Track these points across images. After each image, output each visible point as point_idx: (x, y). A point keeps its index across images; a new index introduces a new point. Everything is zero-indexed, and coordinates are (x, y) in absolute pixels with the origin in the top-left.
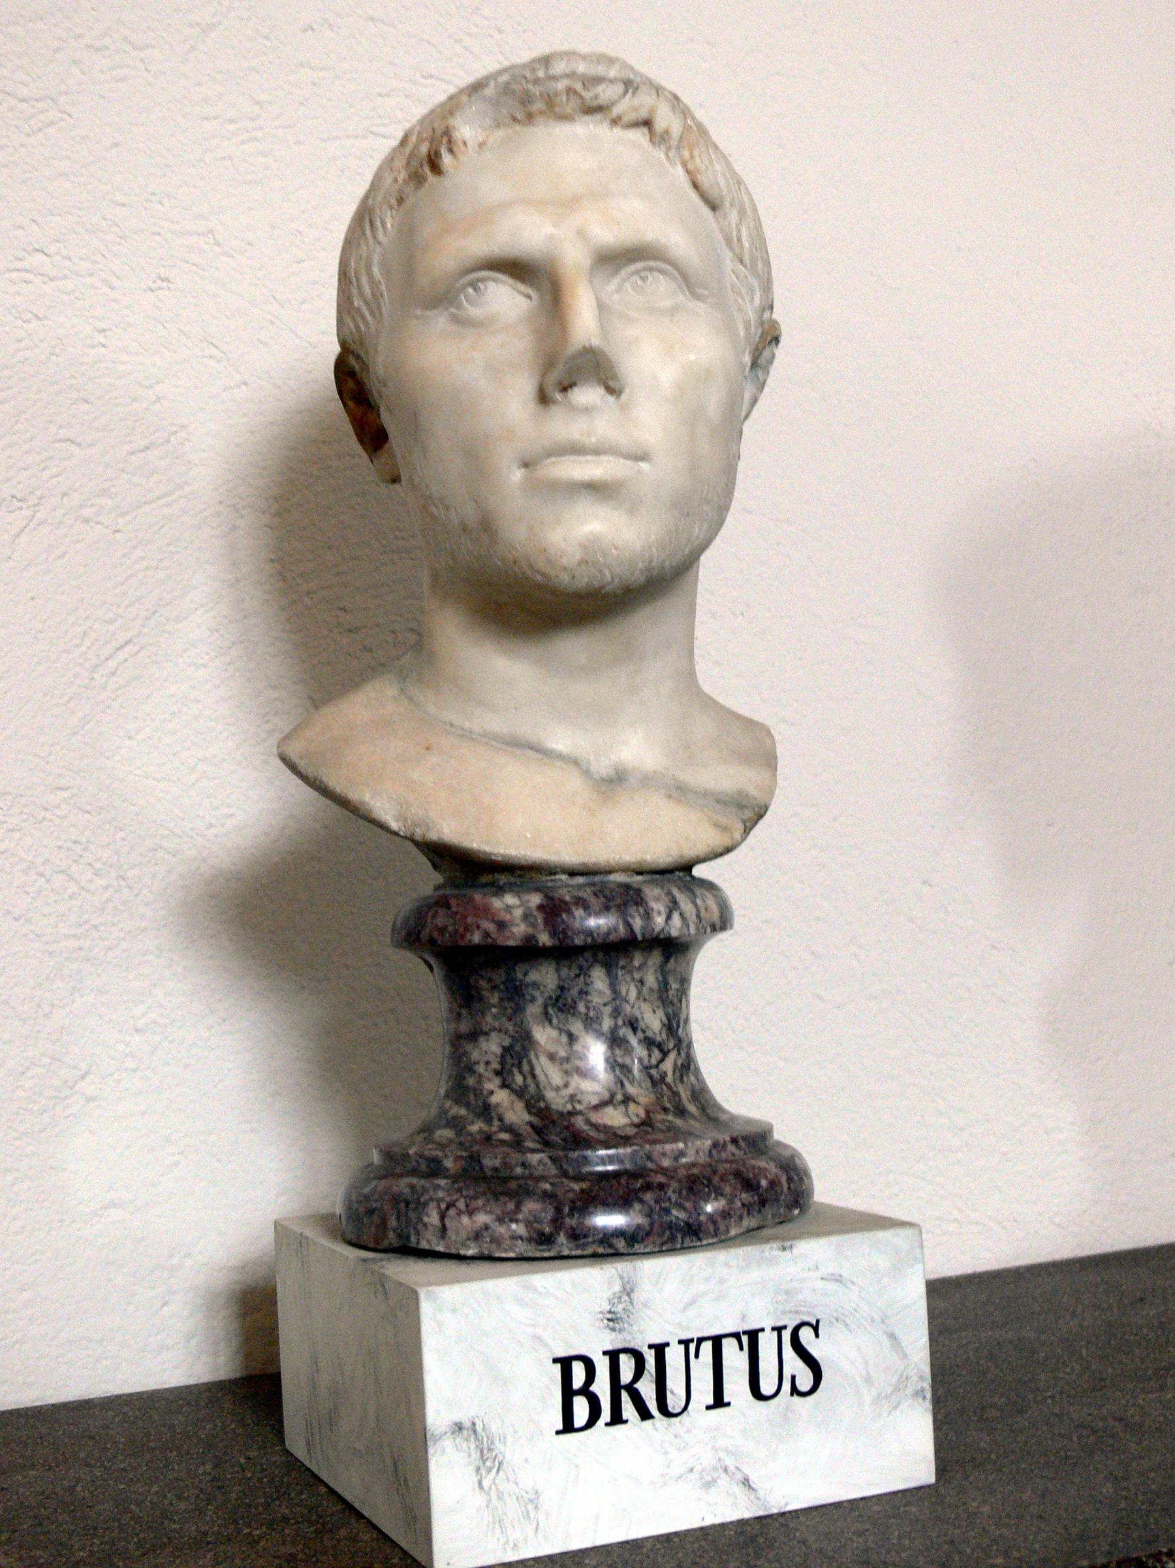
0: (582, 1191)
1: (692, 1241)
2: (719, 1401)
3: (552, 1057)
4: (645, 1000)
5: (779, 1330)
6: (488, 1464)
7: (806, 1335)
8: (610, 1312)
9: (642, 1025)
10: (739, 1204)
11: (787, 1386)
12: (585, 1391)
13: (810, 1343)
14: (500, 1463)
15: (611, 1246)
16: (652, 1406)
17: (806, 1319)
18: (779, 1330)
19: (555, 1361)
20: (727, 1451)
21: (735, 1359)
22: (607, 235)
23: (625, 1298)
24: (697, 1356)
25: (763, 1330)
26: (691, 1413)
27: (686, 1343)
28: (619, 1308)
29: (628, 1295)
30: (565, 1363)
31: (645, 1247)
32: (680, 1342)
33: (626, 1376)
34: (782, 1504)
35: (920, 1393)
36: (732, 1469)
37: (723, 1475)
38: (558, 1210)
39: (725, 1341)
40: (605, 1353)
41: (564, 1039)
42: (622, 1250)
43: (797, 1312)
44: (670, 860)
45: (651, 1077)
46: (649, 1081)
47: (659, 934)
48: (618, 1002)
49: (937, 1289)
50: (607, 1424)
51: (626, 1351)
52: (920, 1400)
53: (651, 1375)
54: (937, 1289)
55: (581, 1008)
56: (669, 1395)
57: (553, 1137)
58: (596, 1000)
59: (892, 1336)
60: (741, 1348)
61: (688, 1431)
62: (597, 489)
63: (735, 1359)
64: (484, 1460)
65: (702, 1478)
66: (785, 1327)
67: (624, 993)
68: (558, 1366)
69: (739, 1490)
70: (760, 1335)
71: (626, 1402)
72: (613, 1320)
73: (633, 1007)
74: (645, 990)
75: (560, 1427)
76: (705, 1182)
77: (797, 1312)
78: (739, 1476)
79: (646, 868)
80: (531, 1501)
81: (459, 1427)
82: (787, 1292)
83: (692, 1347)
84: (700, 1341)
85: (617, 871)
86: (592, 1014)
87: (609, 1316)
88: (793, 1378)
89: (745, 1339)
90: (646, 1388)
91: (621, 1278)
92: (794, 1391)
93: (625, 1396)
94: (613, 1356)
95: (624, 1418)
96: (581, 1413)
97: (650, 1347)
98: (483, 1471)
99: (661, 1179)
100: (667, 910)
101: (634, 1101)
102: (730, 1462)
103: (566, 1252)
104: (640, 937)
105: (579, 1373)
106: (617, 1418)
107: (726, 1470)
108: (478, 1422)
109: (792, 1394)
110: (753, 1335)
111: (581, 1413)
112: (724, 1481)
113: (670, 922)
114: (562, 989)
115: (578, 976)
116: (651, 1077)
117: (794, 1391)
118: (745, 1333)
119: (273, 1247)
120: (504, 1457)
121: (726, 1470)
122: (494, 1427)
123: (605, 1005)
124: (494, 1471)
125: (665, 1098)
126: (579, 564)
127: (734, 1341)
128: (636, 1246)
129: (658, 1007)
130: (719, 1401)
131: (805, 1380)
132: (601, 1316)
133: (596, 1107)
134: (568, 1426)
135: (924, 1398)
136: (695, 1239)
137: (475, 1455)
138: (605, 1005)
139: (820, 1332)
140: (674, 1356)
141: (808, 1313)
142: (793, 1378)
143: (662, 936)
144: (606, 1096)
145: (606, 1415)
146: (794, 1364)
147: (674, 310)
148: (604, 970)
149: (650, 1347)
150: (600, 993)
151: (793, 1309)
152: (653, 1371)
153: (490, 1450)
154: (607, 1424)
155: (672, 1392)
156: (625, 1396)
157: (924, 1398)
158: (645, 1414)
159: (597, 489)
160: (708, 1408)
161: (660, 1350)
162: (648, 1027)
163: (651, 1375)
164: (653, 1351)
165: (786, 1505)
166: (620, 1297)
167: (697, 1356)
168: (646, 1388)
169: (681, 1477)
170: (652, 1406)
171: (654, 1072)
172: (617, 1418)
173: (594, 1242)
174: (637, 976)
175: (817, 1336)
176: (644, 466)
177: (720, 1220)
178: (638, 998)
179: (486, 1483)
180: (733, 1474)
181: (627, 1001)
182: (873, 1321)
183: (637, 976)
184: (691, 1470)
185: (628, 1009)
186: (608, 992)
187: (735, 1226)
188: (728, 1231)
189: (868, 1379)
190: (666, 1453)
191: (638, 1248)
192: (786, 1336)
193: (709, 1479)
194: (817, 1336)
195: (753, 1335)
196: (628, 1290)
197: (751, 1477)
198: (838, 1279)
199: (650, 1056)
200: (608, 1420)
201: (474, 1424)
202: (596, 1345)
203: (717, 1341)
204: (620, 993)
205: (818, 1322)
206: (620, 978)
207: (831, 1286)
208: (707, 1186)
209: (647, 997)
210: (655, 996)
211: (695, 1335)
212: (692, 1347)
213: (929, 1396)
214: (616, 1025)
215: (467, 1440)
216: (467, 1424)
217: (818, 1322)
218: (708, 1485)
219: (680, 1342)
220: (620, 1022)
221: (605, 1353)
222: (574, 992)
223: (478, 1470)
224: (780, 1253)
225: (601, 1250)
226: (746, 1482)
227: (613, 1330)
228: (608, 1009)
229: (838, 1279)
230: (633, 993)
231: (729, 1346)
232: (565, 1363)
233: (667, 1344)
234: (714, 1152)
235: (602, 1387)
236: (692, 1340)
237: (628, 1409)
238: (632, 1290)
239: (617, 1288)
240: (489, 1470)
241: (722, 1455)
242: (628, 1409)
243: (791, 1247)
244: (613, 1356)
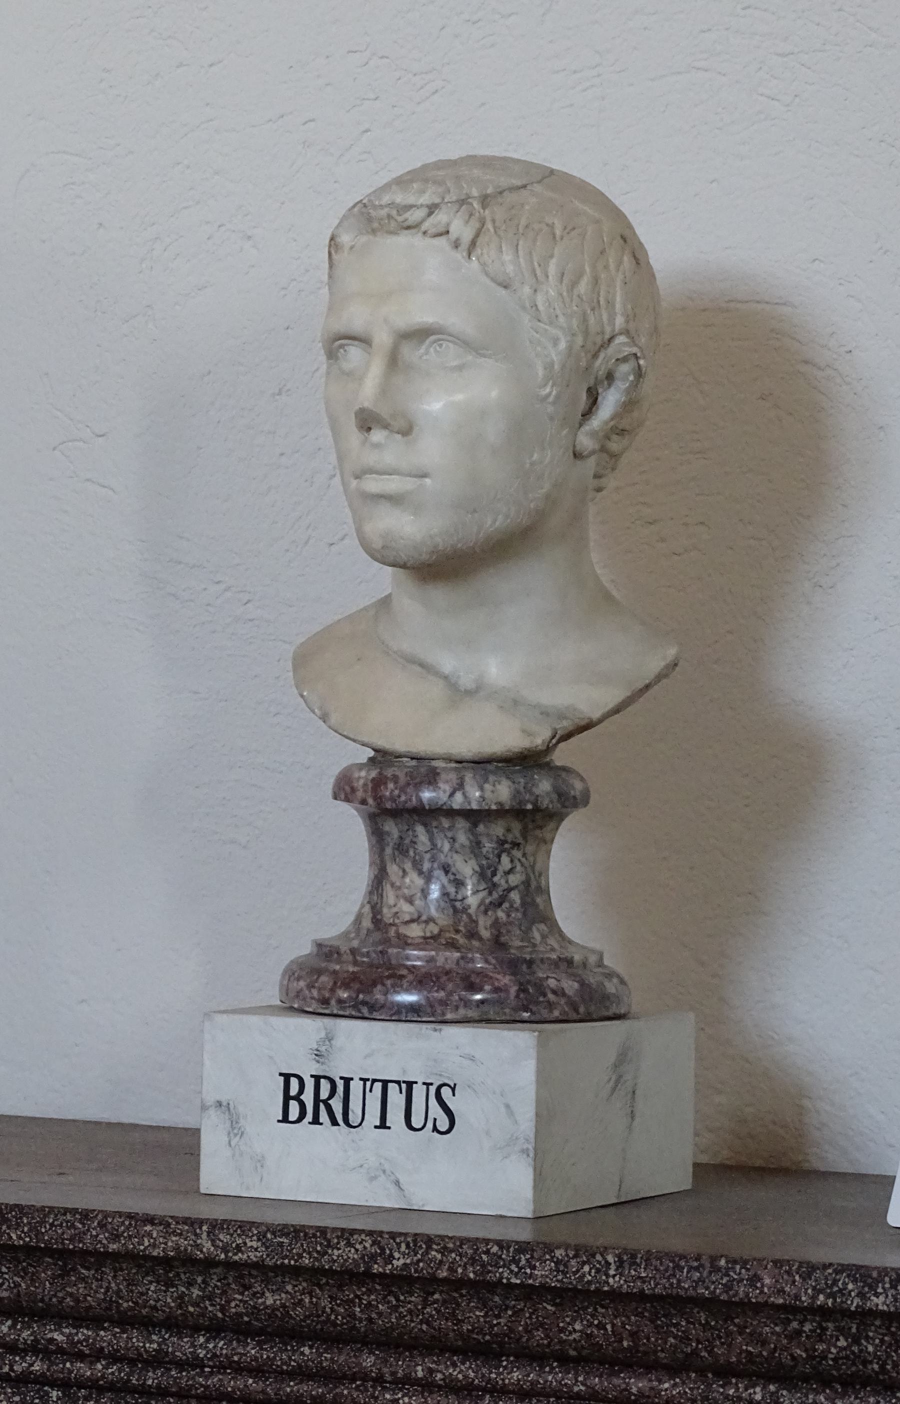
0: (353, 972)
1: (413, 1017)
2: (383, 1125)
3: (392, 885)
4: (457, 852)
6: (235, 1131)
7: (446, 1092)
8: (318, 1050)
9: (453, 870)
10: (457, 998)
11: (430, 1125)
12: (297, 1098)
13: (447, 1098)
14: (242, 1133)
15: (359, 1011)
16: (339, 1118)
17: (447, 1081)
18: (428, 1085)
19: (281, 1074)
20: (386, 1159)
21: (396, 1098)
22: (402, 322)
23: (327, 1043)
24: (371, 1091)
25: (416, 1083)
26: (365, 1128)
27: (365, 1080)
28: (323, 1049)
29: (329, 1041)
30: (287, 1077)
31: (381, 1015)
32: (361, 1079)
33: (324, 1094)
34: (421, 1204)
35: (525, 1151)
36: (388, 1172)
37: (383, 1176)
38: (335, 983)
39: (390, 1085)
40: (312, 1076)
41: (401, 873)
42: (367, 1015)
43: (440, 1075)
44: (470, 754)
45: (454, 907)
46: (452, 910)
47: (442, 805)
48: (435, 851)
50: (310, 1123)
51: (325, 1077)
52: (525, 1156)
53: (340, 1097)
55: (411, 853)
56: (350, 1113)
58: (420, 848)
59: (507, 1106)
60: (401, 1092)
61: (361, 1140)
62: (394, 500)
63: (396, 1098)
64: (233, 1128)
65: (368, 1173)
66: (432, 1084)
67: (439, 845)
68: (282, 1078)
69: (393, 1188)
70: (414, 1085)
71: (323, 1111)
72: (318, 1055)
73: (446, 856)
74: (457, 845)
76: (434, 979)
77: (440, 1075)
78: (393, 1178)
79: (453, 757)
80: (259, 1161)
81: (219, 1104)
82: (435, 1061)
83: (368, 1084)
84: (374, 1081)
85: (439, 759)
86: (417, 858)
87: (316, 1052)
89: (404, 1086)
90: (337, 1104)
91: (326, 1029)
92: (435, 1129)
93: (322, 1107)
94: (317, 1079)
95: (321, 1121)
96: (294, 1110)
97: (341, 1078)
98: (232, 1135)
99: (404, 972)
100: (452, 789)
101: (435, 923)
102: (387, 1166)
103: (335, 1012)
104: (427, 807)
105: (294, 1084)
106: (316, 1121)
107: (384, 1171)
108: (231, 1103)
109: (433, 1131)
110: (410, 1085)
111: (294, 1110)
112: (382, 1178)
113: (452, 799)
114: (401, 838)
115: (408, 830)
116: (454, 907)
117: (435, 1129)
118: (404, 1082)
120: (245, 1129)
121: (384, 1171)
122: (241, 1109)
123: (426, 852)
124: (238, 1136)
125: (462, 924)
126: (383, 548)
128: (375, 1013)
129: (470, 859)
130: (383, 1125)
131: (443, 1125)
132: (311, 1051)
133: (407, 923)
134: (285, 1119)
135: (528, 1155)
136: (416, 1015)
137: (228, 1124)
138: (426, 852)
139: (456, 1092)
140: (356, 1087)
141: (449, 1078)
143: (445, 807)
144: (415, 916)
145: (309, 1117)
146: (435, 1110)
147: (460, 368)
148: (423, 827)
149: (341, 1078)
150: (423, 844)
151: (439, 1073)
152: (342, 1094)
153: (237, 1122)
155: (353, 1111)
156: (322, 1107)
157: (528, 1155)
158: (334, 1123)
159: (394, 500)
160: (376, 1127)
161: (347, 1081)
162: (459, 872)
163: (340, 1097)
164: (342, 1081)
165: (423, 1205)
166: (324, 1041)
167: (371, 1091)
168: (337, 1104)
169: (354, 1169)
170: (339, 1118)
171: (458, 904)
172: (316, 1121)
173: (349, 1007)
174: (449, 834)
175: (454, 1095)
176: (428, 481)
177: (436, 1005)
178: (450, 850)
179: (233, 1143)
180: (390, 1176)
181: (442, 852)
182: (494, 1093)
183: (449, 834)
184: (361, 1166)
185: (442, 857)
186: (429, 843)
187: (451, 1013)
188: (444, 1014)
189: (488, 1133)
190: (346, 1151)
191: (376, 1015)
192: (433, 1089)
193: (373, 1175)
194: (454, 1095)
195: (410, 1085)
196: (329, 1038)
197: (401, 1181)
198: (472, 1059)
199: (457, 892)
200: (311, 1120)
201: (229, 1104)
202: (307, 1069)
203: (385, 1083)
204: (436, 845)
205: (455, 1085)
206: (436, 834)
207: (466, 1062)
208: (434, 982)
209: (459, 850)
210: (468, 850)
211: (371, 1077)
212: (368, 1084)
213: (532, 1155)
214: (432, 867)
215: (224, 1113)
216: (225, 1104)
217: (455, 1085)
218: (373, 1179)
219: (361, 1079)
220: (436, 865)
221: (312, 1076)
222: (407, 841)
223: (229, 1134)
224: (432, 1032)
225: (353, 1013)
226: (397, 1183)
227: (318, 1062)
228: (428, 856)
229: (472, 1059)
230: (447, 846)
231: (392, 1088)
232: (287, 1077)
233: (352, 1079)
234: (462, 963)
235: (308, 1097)
236: (368, 1080)
237: (324, 1116)
238: (332, 1039)
239: (323, 1035)
240: (236, 1135)
241: (382, 1161)
242: (324, 1116)
243: (441, 1030)
244: (317, 1079)
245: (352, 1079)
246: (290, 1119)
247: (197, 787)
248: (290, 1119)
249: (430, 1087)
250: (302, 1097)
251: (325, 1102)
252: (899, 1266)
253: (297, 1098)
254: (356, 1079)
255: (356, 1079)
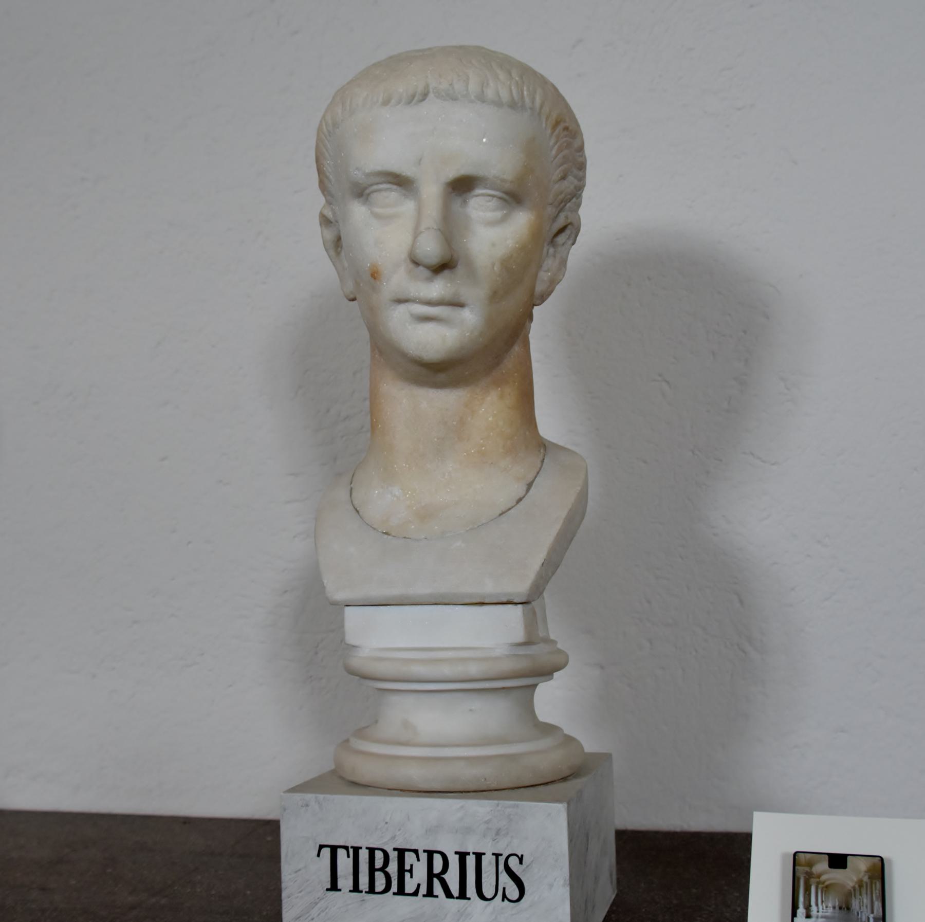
5: (497, 856)
7: (513, 863)
18: (497, 856)
21: (345, 863)
24: (419, 885)
39: (407, 854)
40: (456, 853)
49: (271, 828)
50: (424, 896)
54: (271, 828)
57: (517, 79)
60: (348, 856)
68: (426, 854)
75: (329, 887)
84: (415, 893)
88: (504, 889)
89: (351, 851)
93: (436, 882)
96: (380, 884)
97: (395, 849)
109: (503, 900)
110: (356, 850)
111: (380, 884)
117: (504, 897)
118: (352, 847)
119: (348, 643)
127: (413, 855)
131: (513, 892)
142: (504, 889)
145: (394, 888)
146: (504, 878)
149: (395, 849)
154: (424, 896)
158: (449, 894)
167: (419, 885)
175: (521, 863)
192: (502, 860)
195: (356, 850)
203: (334, 849)
221: (456, 853)
231: (341, 853)
233: (361, 848)
235: (393, 868)
245: (361, 848)
246: (406, 891)
247: (471, 710)
248: (406, 891)
249: (500, 857)
250: (445, 876)
251: (439, 876)
252: (288, 915)
253: (383, 869)
254: (364, 848)
255: (364, 848)
